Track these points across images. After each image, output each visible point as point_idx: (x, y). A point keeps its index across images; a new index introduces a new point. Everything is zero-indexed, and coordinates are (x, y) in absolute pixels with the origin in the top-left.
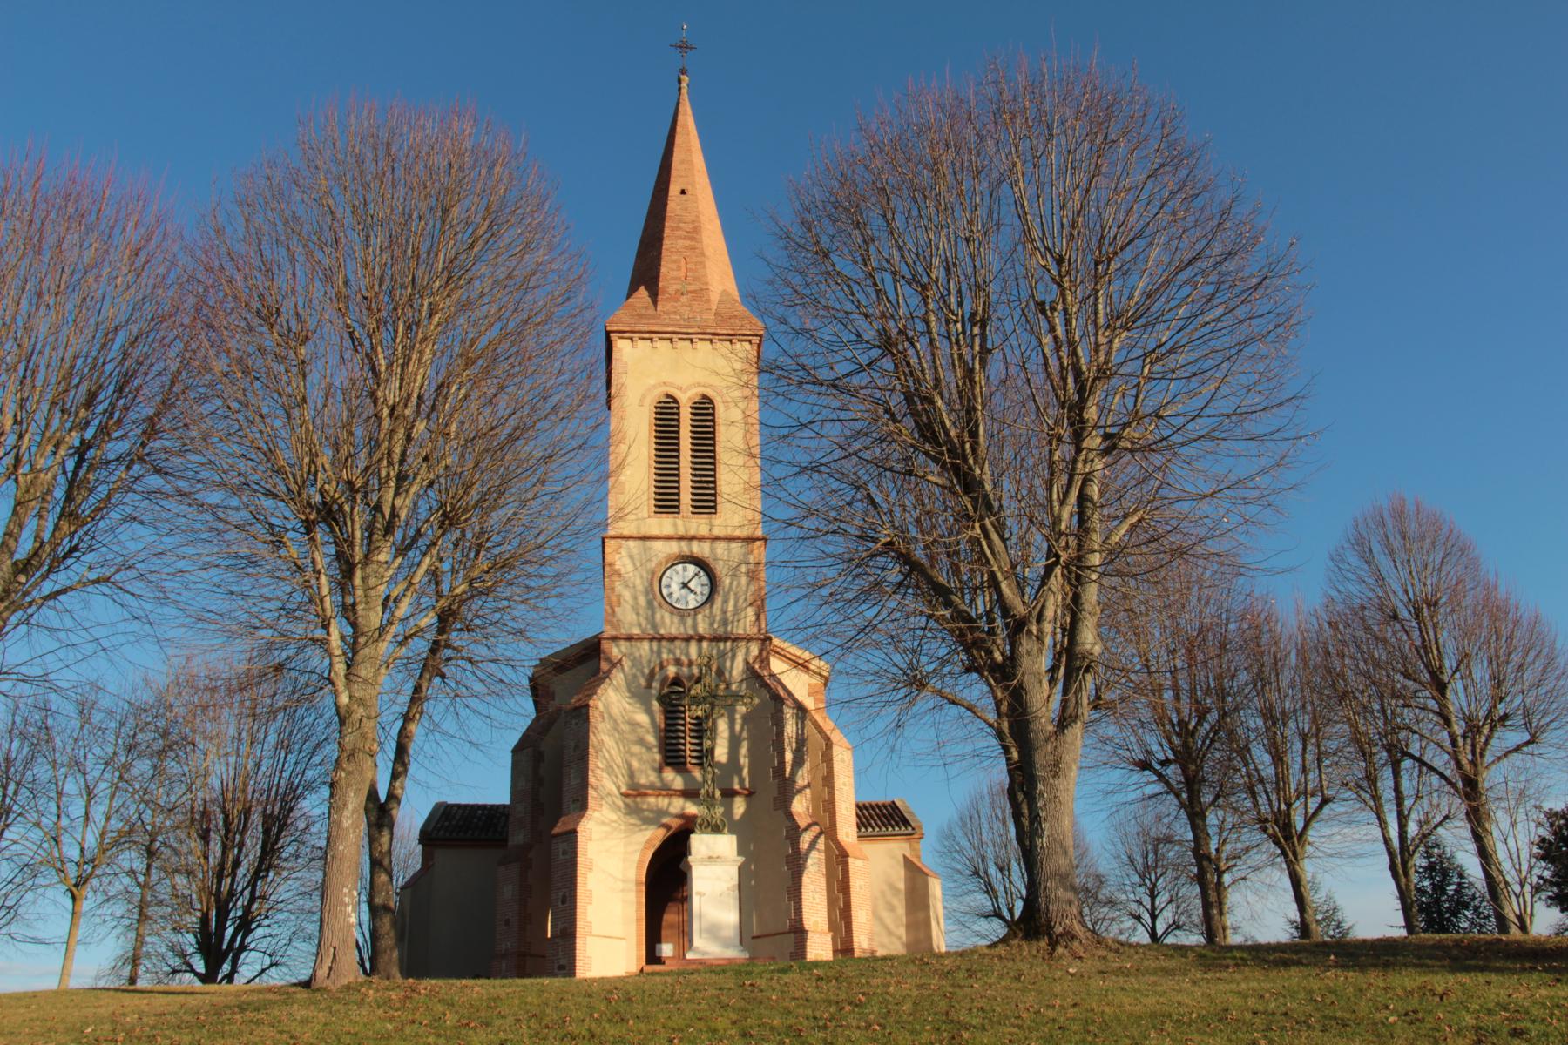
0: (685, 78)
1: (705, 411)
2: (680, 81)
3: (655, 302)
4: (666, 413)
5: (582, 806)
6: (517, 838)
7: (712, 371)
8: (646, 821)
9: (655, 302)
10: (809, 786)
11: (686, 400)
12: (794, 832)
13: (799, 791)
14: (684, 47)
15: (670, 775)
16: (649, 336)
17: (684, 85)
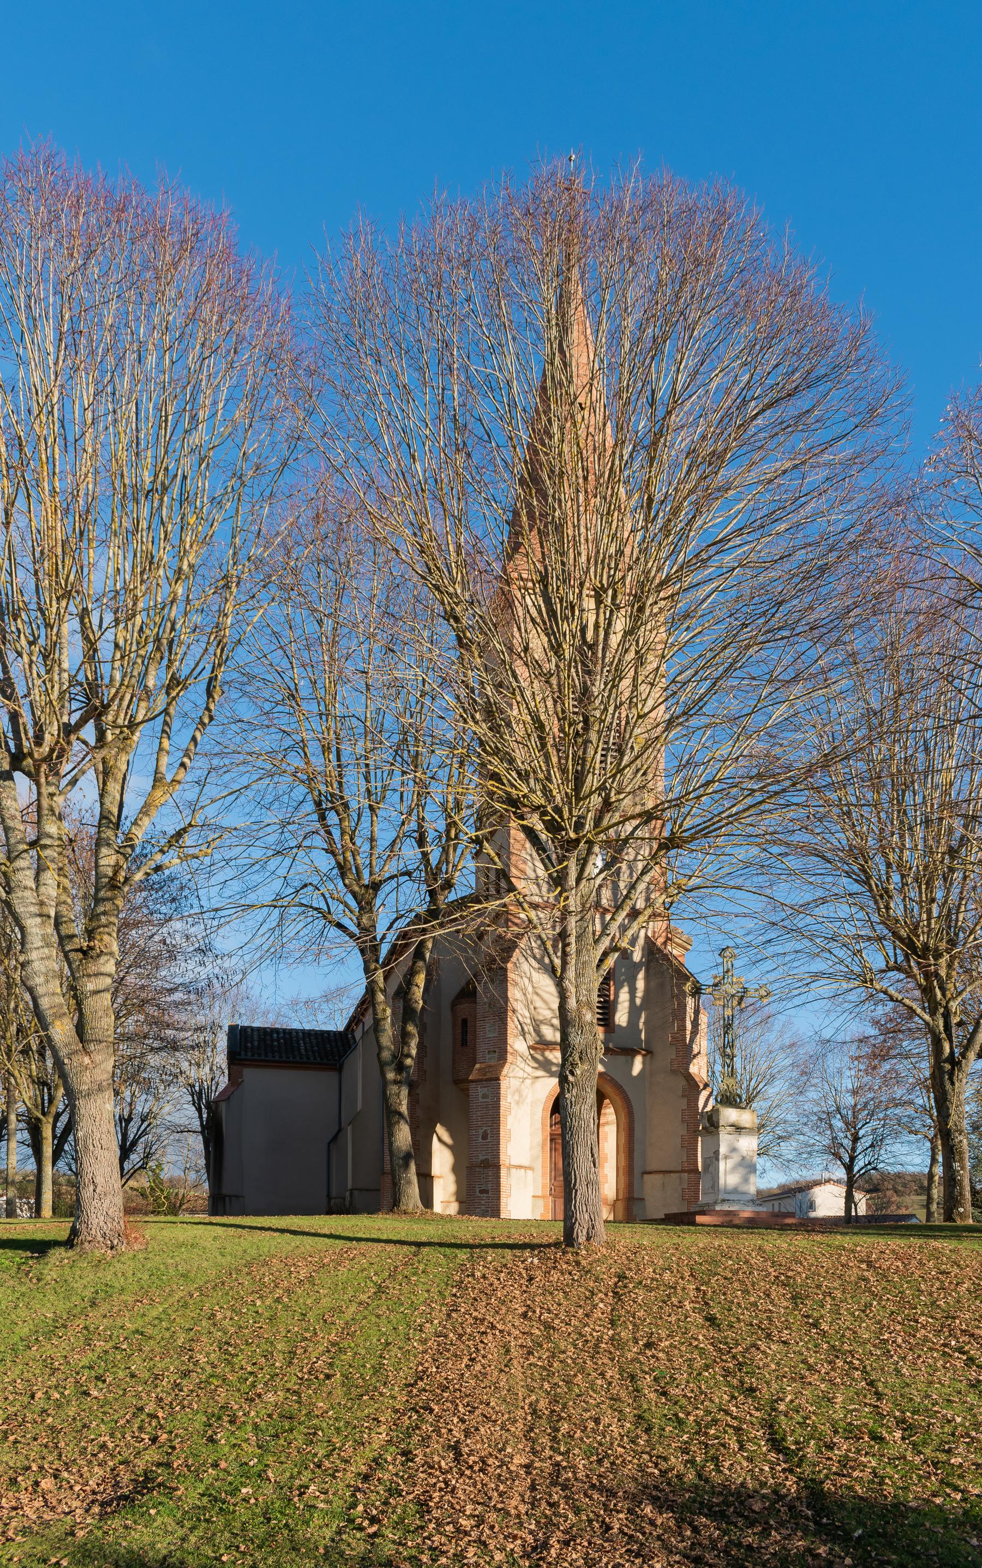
13: (695, 1056)
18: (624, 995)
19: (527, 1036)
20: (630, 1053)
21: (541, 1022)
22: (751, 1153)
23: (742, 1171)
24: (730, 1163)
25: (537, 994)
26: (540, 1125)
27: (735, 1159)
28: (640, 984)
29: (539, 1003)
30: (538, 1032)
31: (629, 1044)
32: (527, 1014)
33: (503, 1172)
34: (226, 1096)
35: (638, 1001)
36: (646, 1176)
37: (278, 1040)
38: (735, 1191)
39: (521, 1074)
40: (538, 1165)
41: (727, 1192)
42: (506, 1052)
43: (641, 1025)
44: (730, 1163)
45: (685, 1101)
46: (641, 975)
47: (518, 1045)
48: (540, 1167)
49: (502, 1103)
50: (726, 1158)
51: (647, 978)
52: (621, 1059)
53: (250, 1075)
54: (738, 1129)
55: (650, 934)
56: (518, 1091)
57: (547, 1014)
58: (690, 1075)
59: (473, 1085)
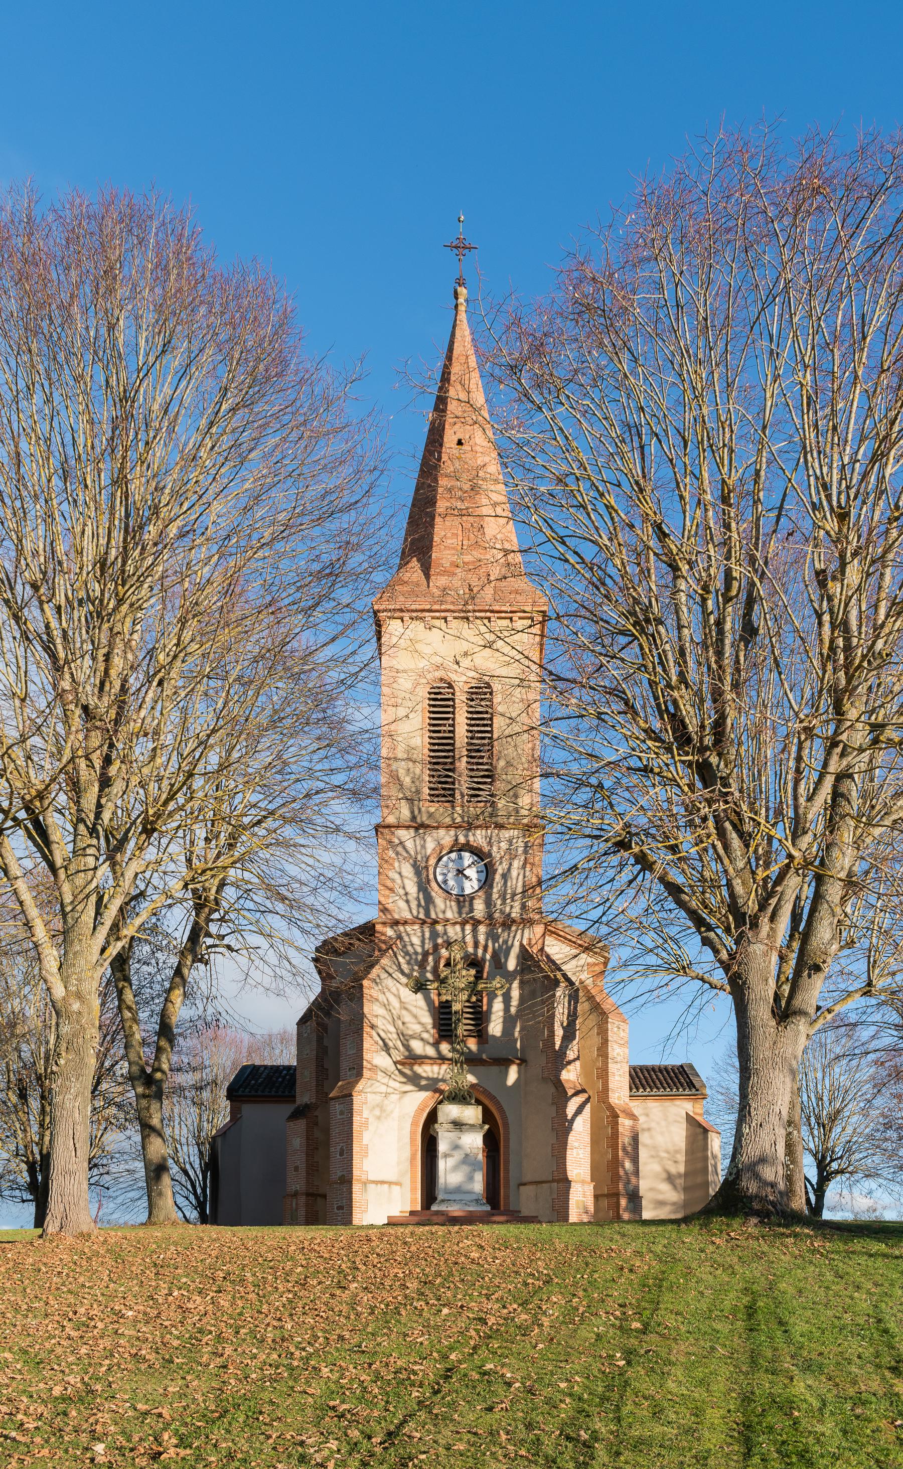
0: (463, 291)
1: (481, 692)
2: (456, 295)
3: (427, 576)
4: (441, 702)
5: (357, 1071)
6: (304, 1097)
7: (493, 656)
8: (422, 1088)
9: (427, 576)
10: (578, 1058)
11: (462, 681)
12: (561, 1095)
13: (569, 1063)
14: (461, 247)
15: (445, 1047)
16: (418, 615)
17: (461, 300)
18: (498, 1006)
19: (392, 1051)
20: (505, 1063)
21: (412, 1037)
22: (475, 1151)
23: (466, 1169)
24: (451, 1162)
25: (406, 1009)
26: (408, 1140)
27: (458, 1156)
28: (515, 993)
29: (407, 1018)
30: (407, 1047)
31: (503, 1054)
32: (393, 1030)
33: (356, 1188)
34: (224, 1133)
35: (513, 1010)
36: (522, 1188)
37: (284, 1078)
38: (458, 1190)
39: (383, 1089)
40: (407, 1181)
41: (448, 1191)
42: (361, 1067)
43: (517, 1034)
44: (451, 1162)
45: (554, 1108)
46: (516, 984)
47: (375, 1057)
48: (409, 1182)
49: (356, 1118)
50: (446, 1156)
51: (521, 987)
52: (495, 1069)
53: (248, 1109)
54: (458, 1125)
55: (525, 942)
56: (381, 1107)
57: (417, 1028)
58: (560, 1081)
59: (332, 1103)
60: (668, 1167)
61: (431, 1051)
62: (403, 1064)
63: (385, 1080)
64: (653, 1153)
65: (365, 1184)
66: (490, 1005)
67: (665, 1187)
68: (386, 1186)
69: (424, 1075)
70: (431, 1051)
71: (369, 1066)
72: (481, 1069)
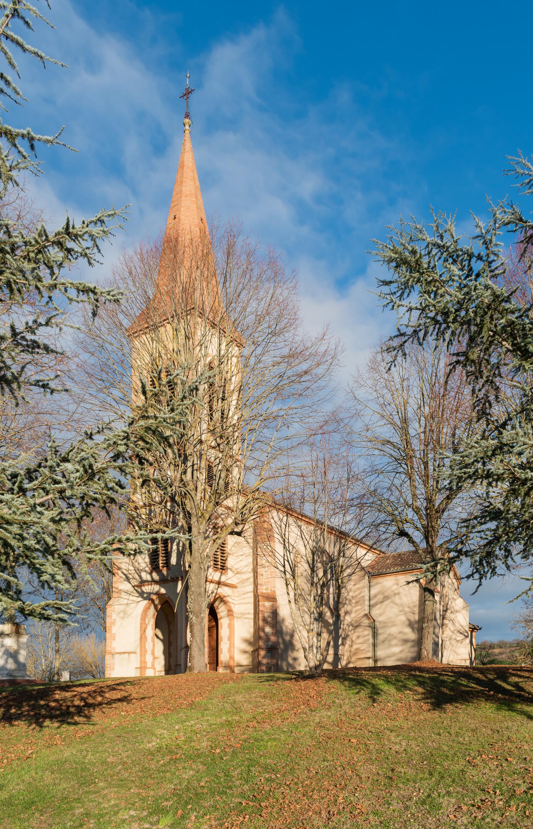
19: (131, 580)
30: (140, 577)
32: (131, 568)
56: (124, 612)
60: (409, 618)
61: (149, 578)
62: (137, 586)
63: (127, 597)
64: (401, 609)
65: (113, 654)
66: (172, 548)
67: (408, 630)
68: (127, 655)
69: (145, 591)
70: (149, 578)
71: (116, 590)
72: (167, 585)
